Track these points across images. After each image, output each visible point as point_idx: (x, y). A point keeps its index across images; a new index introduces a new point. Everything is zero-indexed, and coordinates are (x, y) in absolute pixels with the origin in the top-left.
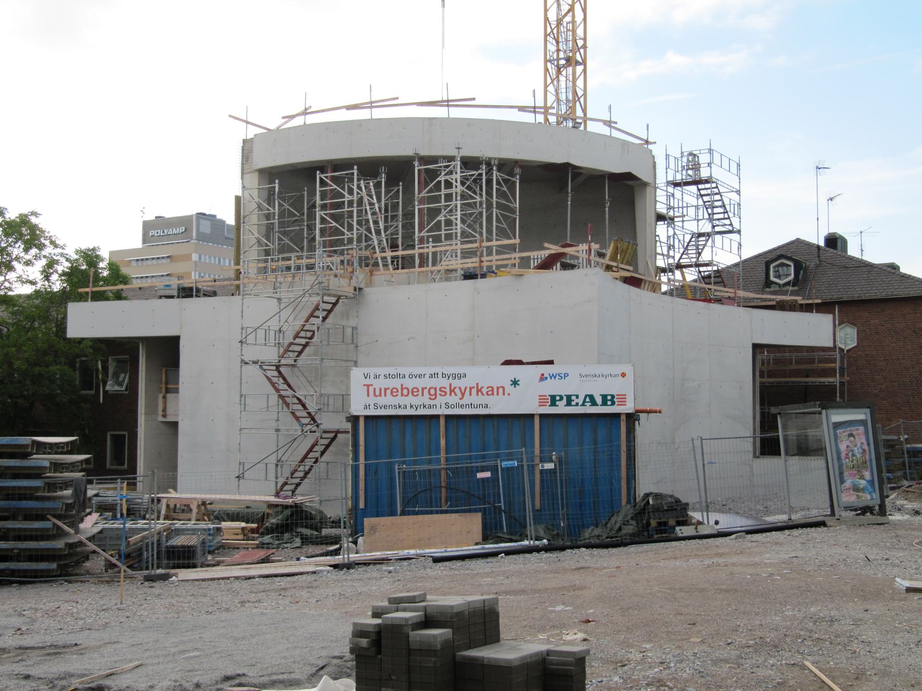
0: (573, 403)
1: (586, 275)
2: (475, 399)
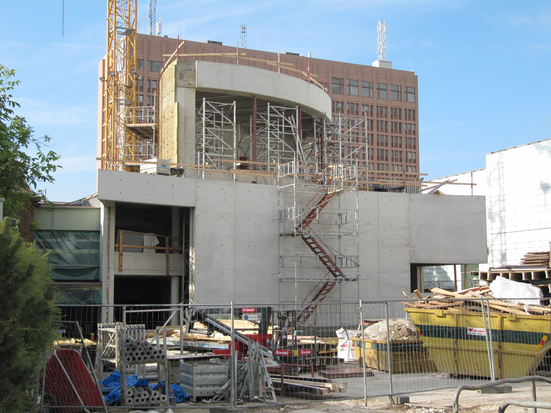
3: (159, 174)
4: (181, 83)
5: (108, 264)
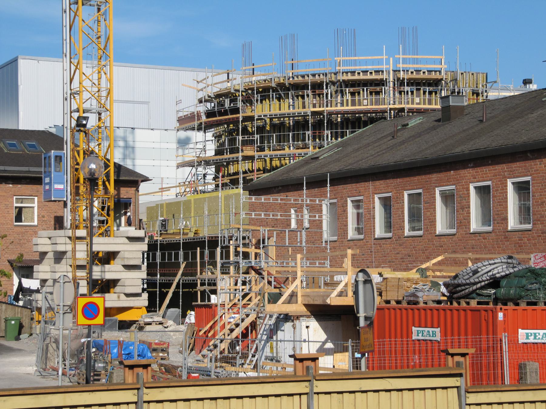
0: (537, 338)
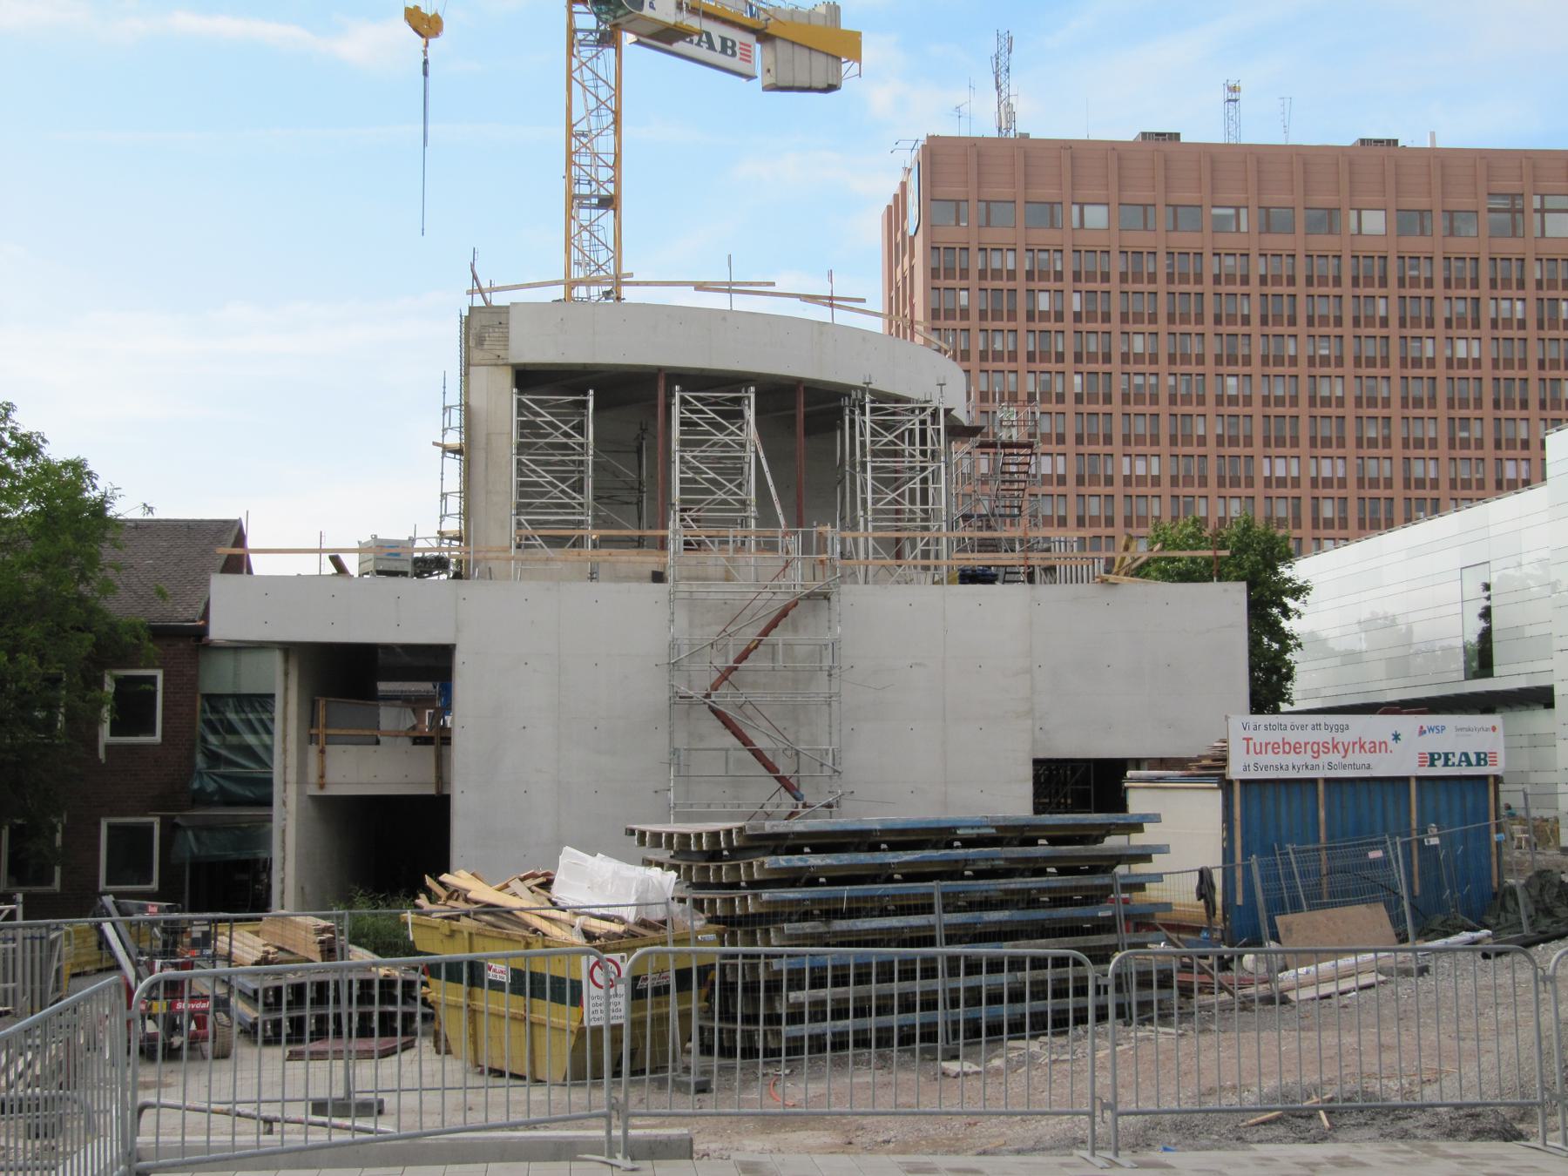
1: (1226, 591)
2: (1356, 757)
3: (379, 573)
4: (477, 355)
5: (285, 773)
